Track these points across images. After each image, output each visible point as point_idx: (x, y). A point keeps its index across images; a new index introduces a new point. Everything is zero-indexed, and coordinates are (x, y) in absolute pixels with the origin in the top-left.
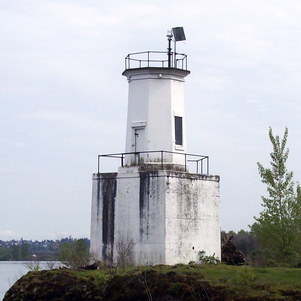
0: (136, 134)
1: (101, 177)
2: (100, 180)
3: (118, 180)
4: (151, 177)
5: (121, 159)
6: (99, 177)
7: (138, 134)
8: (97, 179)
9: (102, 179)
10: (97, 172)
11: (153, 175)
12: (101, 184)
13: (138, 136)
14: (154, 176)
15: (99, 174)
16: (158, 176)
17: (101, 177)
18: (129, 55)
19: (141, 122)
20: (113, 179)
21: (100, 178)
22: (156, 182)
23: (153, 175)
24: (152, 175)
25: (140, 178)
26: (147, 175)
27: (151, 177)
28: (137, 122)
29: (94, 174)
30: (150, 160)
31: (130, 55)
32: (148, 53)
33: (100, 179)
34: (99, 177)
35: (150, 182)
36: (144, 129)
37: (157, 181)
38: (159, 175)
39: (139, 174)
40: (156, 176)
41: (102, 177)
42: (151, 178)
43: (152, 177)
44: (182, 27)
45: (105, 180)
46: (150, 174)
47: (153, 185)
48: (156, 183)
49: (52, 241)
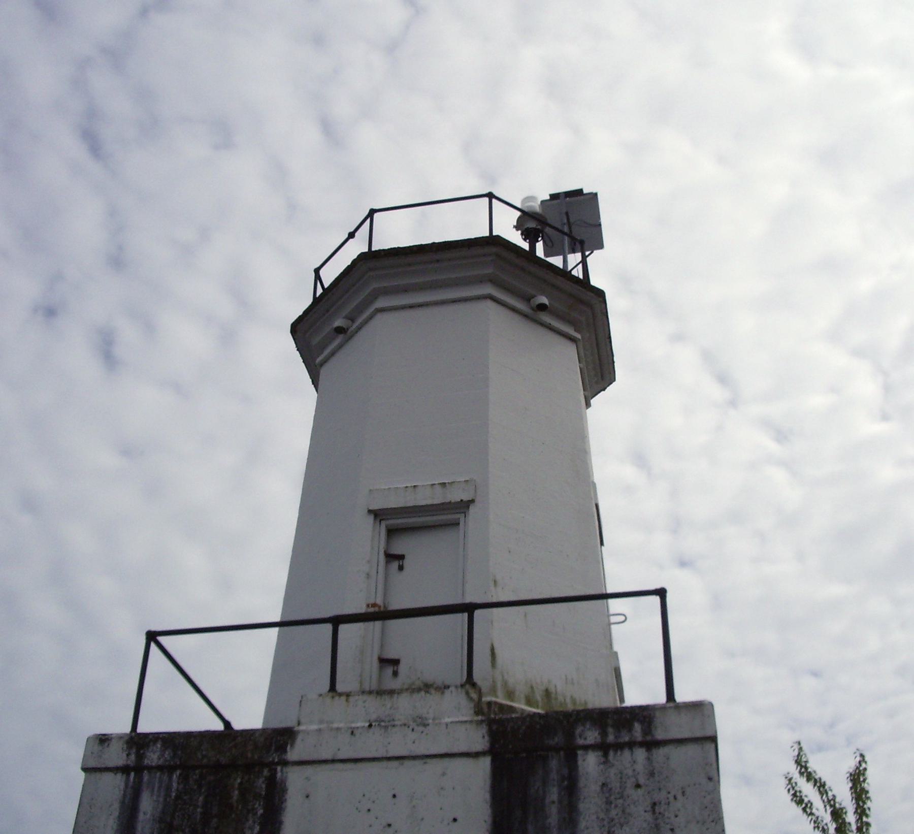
0: (391, 557)
1: (153, 757)
2: (146, 776)
3: (295, 781)
4: (586, 748)
5: (343, 628)
6: (140, 757)
7: (401, 557)
8: (124, 770)
9: (160, 768)
10: (127, 729)
11: (611, 738)
12: (148, 805)
13: (401, 568)
14: (619, 747)
15: (138, 741)
16: (651, 745)
17: (153, 757)
18: (372, 212)
19: (443, 485)
20: (250, 768)
21: (146, 762)
22: (638, 786)
23: (611, 738)
24: (604, 734)
25: (486, 763)
26: (558, 739)
27: (586, 748)
28: (409, 481)
29: (103, 740)
30: (505, 684)
31: (376, 215)
32: (486, 200)
33: (150, 768)
34: (140, 757)
35: (581, 783)
36: (456, 524)
37: (652, 774)
38: (660, 735)
39: (484, 730)
40: (631, 745)
41: (168, 754)
42: (590, 763)
43: (604, 748)
44: (596, 194)
45: (184, 778)
46: (578, 731)
47: (609, 802)
48: (640, 792)
49: (551, 195)
